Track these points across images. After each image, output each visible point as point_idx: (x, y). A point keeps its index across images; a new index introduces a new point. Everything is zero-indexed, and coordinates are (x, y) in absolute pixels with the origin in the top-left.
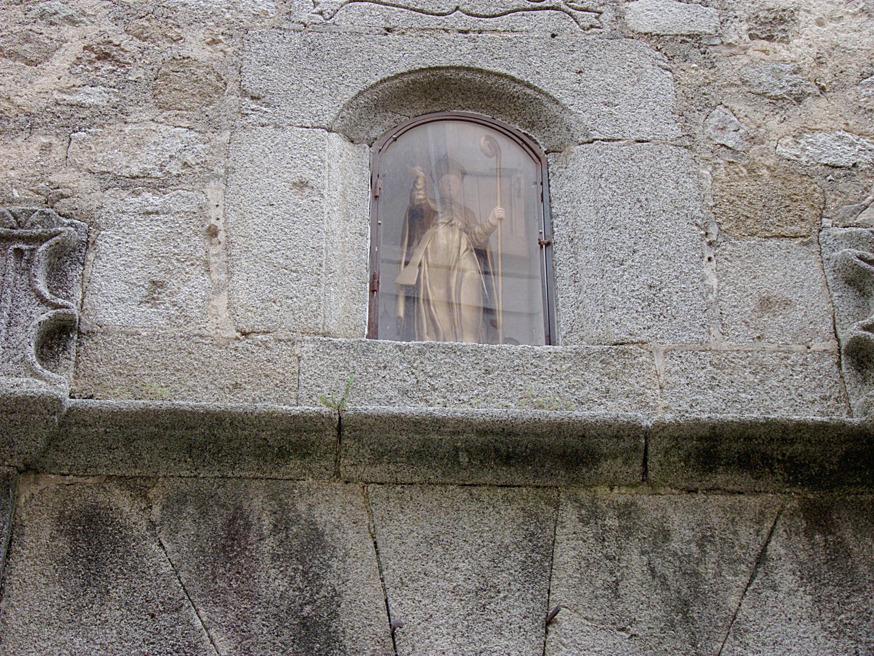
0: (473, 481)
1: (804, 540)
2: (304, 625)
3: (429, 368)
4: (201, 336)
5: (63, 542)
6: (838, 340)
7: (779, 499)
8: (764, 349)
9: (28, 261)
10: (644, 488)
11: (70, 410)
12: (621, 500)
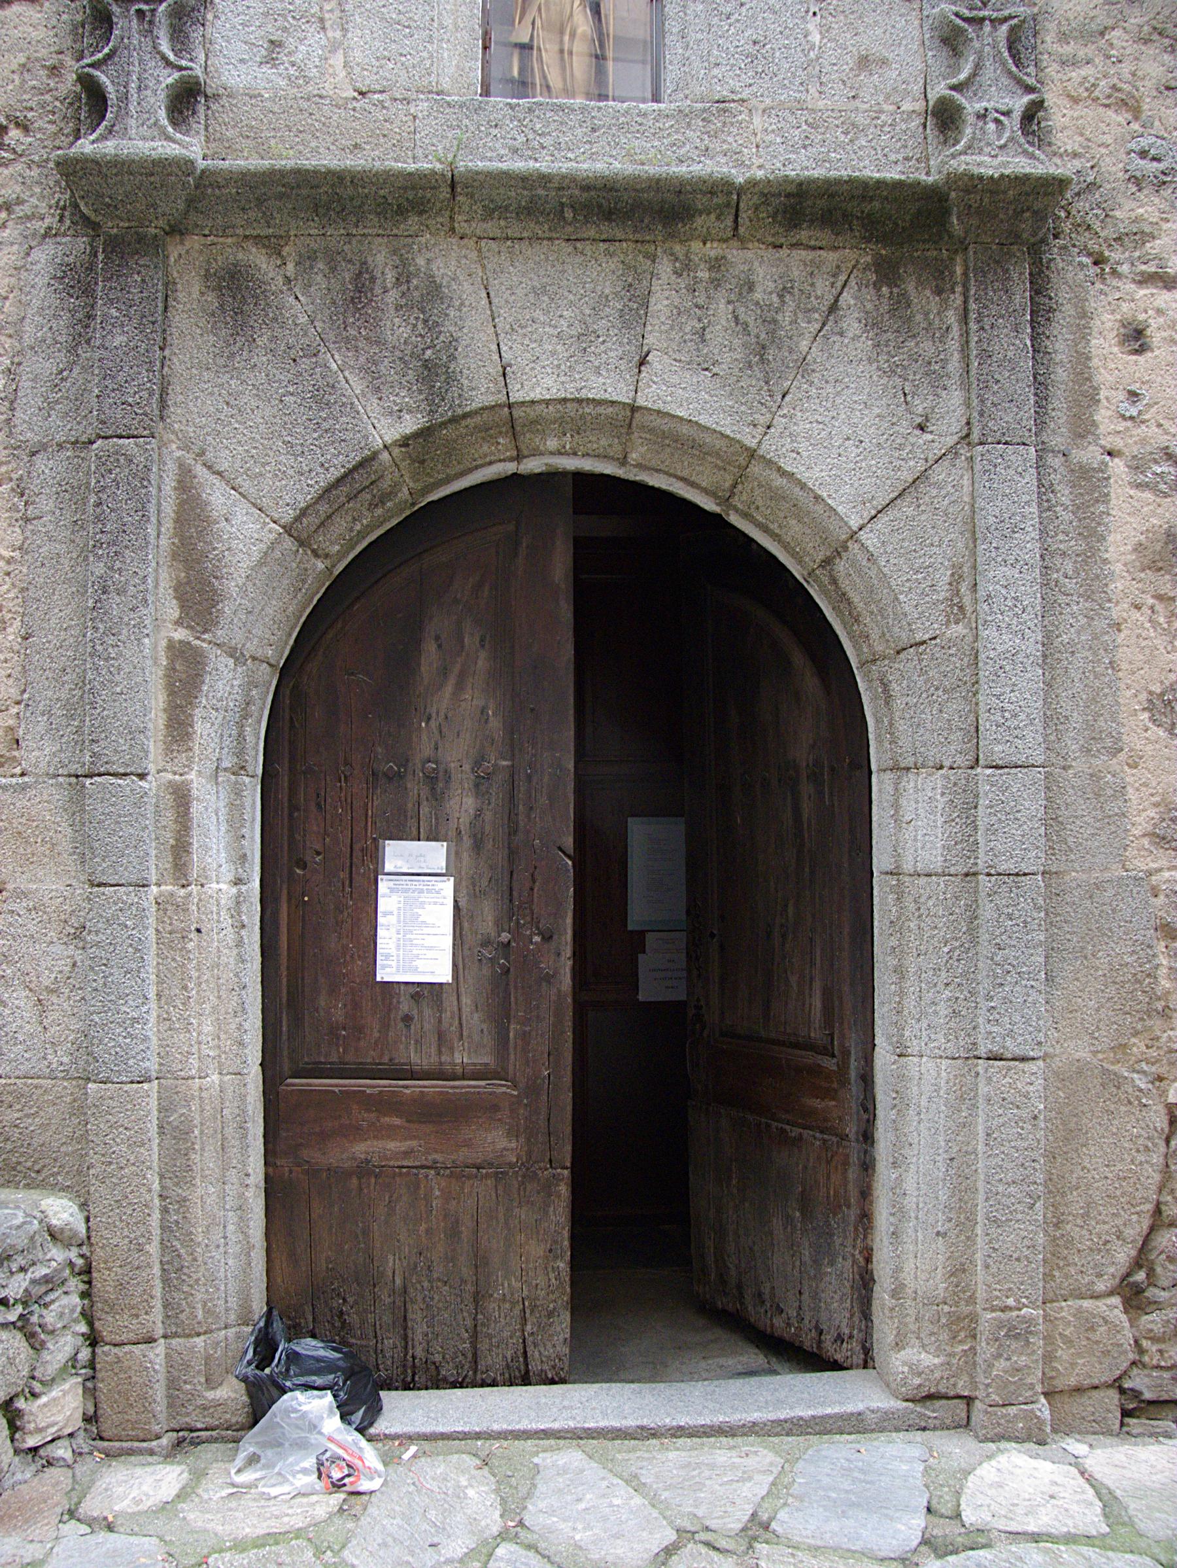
0: (578, 236)
1: (873, 292)
2: (426, 367)
3: (538, 126)
4: (321, 97)
5: (211, 297)
6: (927, 101)
7: (854, 255)
8: (857, 109)
9: (151, 22)
10: (735, 243)
11: (203, 172)
12: (713, 254)
